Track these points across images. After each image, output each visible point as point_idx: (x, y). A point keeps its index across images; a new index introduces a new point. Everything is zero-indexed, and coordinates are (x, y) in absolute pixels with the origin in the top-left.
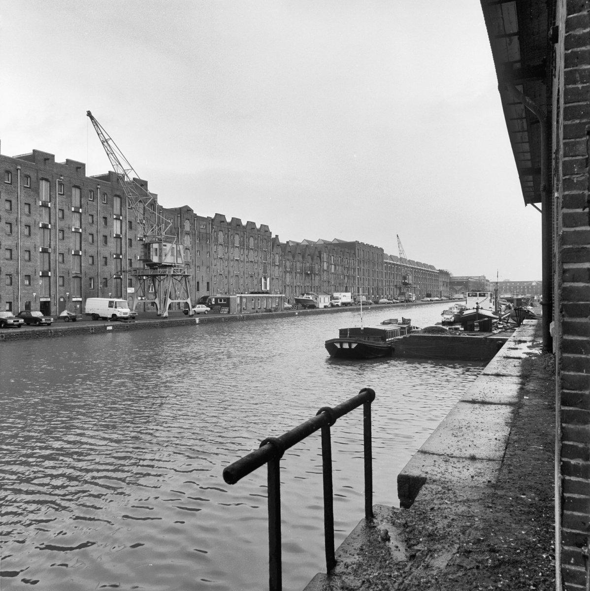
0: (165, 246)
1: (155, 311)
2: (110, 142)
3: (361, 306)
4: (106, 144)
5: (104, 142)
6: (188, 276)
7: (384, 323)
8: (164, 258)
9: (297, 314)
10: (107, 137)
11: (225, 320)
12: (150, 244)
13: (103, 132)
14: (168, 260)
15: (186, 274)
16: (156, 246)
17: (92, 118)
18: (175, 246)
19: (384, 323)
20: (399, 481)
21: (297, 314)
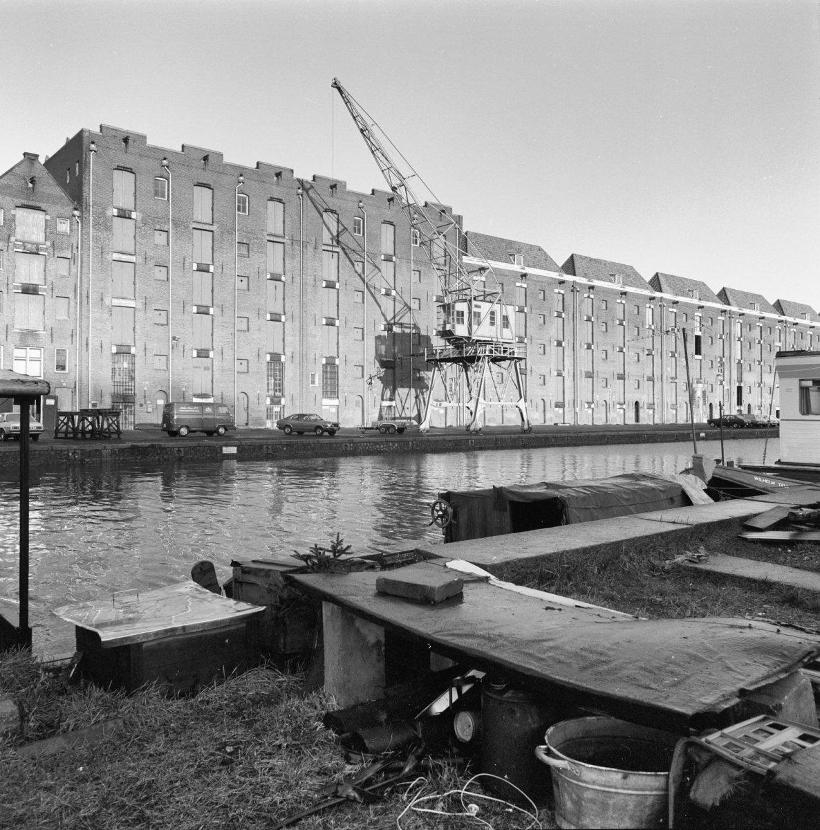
14: (483, 331)
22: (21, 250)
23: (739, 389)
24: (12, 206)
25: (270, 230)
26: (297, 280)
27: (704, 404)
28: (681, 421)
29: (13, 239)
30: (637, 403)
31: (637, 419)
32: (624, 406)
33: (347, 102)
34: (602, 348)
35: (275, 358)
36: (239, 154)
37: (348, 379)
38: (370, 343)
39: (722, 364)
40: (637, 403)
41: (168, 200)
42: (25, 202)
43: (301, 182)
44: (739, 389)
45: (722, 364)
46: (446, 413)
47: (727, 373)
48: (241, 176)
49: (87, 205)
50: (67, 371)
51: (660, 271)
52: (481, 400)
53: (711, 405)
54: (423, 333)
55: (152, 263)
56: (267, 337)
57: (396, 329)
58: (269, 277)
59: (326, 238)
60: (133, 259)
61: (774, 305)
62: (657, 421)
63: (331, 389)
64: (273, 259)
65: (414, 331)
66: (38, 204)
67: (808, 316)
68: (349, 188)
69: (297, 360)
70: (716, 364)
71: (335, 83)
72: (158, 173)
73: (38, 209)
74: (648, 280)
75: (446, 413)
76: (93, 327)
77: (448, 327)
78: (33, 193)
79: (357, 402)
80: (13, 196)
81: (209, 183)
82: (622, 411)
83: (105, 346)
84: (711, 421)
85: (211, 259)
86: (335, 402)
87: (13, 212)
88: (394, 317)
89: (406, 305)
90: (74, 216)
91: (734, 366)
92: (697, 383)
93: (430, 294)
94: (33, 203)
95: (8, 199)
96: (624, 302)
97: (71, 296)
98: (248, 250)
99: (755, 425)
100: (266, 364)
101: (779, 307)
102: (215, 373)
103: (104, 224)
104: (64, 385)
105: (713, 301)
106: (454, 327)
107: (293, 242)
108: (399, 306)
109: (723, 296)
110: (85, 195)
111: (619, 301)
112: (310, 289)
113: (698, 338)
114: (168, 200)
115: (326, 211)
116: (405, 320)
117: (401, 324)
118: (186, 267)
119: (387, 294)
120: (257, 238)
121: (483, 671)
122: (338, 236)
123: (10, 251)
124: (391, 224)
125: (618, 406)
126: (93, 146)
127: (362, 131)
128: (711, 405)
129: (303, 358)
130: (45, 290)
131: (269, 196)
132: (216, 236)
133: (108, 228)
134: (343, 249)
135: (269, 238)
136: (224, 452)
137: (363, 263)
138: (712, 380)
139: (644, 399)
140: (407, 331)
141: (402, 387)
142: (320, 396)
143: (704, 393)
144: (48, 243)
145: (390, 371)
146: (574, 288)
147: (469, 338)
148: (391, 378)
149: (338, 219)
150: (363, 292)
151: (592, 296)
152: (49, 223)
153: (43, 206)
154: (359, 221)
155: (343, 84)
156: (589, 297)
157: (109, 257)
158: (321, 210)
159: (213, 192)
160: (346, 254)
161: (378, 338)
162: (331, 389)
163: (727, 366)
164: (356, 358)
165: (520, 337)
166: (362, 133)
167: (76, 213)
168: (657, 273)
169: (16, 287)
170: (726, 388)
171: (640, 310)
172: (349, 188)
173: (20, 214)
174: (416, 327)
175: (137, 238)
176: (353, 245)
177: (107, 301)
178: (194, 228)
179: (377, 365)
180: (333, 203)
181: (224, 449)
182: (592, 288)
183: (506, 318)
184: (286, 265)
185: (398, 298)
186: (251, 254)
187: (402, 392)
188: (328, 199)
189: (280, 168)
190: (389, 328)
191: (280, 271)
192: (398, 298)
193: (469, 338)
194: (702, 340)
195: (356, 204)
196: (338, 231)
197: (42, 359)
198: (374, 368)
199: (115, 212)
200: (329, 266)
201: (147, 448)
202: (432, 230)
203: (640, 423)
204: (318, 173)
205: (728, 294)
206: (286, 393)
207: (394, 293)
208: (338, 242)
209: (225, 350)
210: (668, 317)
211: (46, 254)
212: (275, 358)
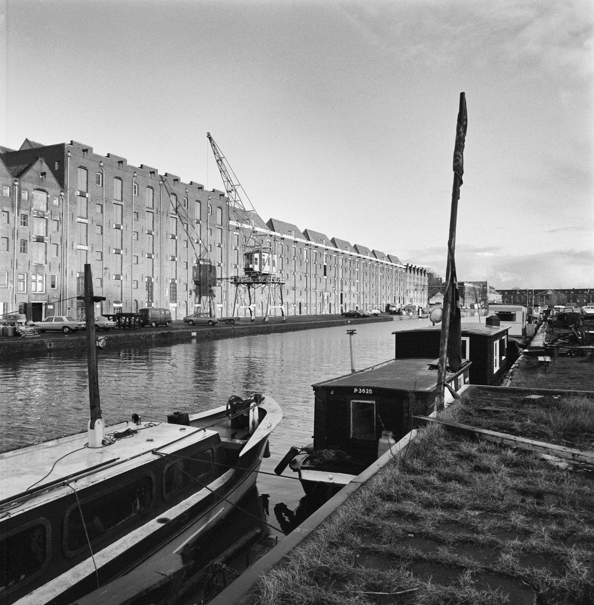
0: (264, 256)
1: (250, 316)
2: (224, 160)
3: (23, 221)
4: (220, 162)
5: (219, 160)
6: (283, 284)
7: (184, 429)
8: (263, 266)
9: (349, 322)
10: (222, 156)
11: (157, 325)
12: (252, 253)
13: (220, 152)
14: (266, 269)
15: (281, 282)
16: (257, 256)
17: (210, 138)
18: (271, 256)
19: (184, 429)
20: (486, 320)
21: (349, 322)
22: (36, 216)
23: (342, 294)
24: (32, 189)
25: (147, 205)
26: (159, 234)
27: (328, 303)
28: (313, 313)
29: (32, 209)
30: (300, 303)
31: (300, 313)
32: (295, 305)
33: (213, 145)
34: (286, 272)
35: (150, 279)
36: (134, 161)
37: (181, 294)
38: (190, 270)
39: (335, 281)
40: (300, 303)
41: (102, 186)
42: (38, 187)
43: (161, 177)
44: (342, 294)
45: (335, 281)
46: (222, 311)
47: (337, 286)
48: (135, 173)
49: (67, 188)
50: (56, 289)
51: (273, 218)
52: (269, 305)
53: (330, 304)
54: (213, 265)
55: (95, 224)
56: (144, 269)
57: (201, 263)
58: (147, 232)
59: (172, 210)
60: (86, 221)
61: (303, 233)
62: (309, 314)
63: (174, 298)
64: (147, 221)
65: (209, 264)
66: (44, 188)
67: (293, 232)
68: (95, 152)
69: (159, 280)
70: (333, 281)
71: (209, 135)
72: (98, 170)
73: (44, 191)
74: (302, 232)
75: (222, 311)
76: (69, 262)
77: (251, 266)
78: (42, 181)
79: (184, 305)
80: (33, 183)
81: (121, 176)
82: (294, 308)
83: (74, 273)
84: (343, 314)
85: (121, 222)
86: (175, 305)
87: (33, 193)
88: (200, 256)
89: (206, 249)
90: (61, 195)
91: (340, 282)
92: (325, 292)
93: (111, 222)
94: (41, 188)
95: (31, 184)
96: (295, 247)
97: (59, 243)
98: (138, 217)
99: (364, 316)
100: (145, 283)
101: (306, 234)
102: (123, 289)
103: (74, 202)
104: (55, 296)
105: (261, 227)
106: (254, 266)
107: (156, 212)
108: (203, 249)
109: (271, 225)
110: (65, 183)
111: (293, 246)
112: (164, 238)
113: (325, 266)
114: (102, 186)
115: (172, 194)
116: (205, 257)
117: (203, 260)
118: (111, 226)
119: (198, 243)
120: (141, 210)
121: (497, 373)
122: (176, 208)
123: (31, 217)
124: (85, 169)
125: (293, 305)
126: (69, 154)
127: (217, 161)
128: (330, 304)
129: (161, 280)
130: (47, 240)
131: (115, 176)
132: (124, 208)
133: (75, 203)
134: (179, 216)
135: (147, 210)
136: (192, 335)
137: (187, 224)
138: (330, 290)
139: (303, 301)
140: (206, 263)
141: (204, 295)
142: (169, 301)
143: (328, 297)
144: (49, 212)
145: (198, 287)
146: (275, 239)
147: (260, 272)
148: (198, 291)
149: (176, 198)
150: (187, 242)
151: (282, 243)
152: (49, 200)
153: (47, 189)
154: (185, 200)
155: (212, 136)
156: (281, 244)
157: (76, 220)
158: (170, 193)
159: (122, 182)
160: (180, 219)
161: (194, 267)
162: (174, 298)
163: (337, 282)
164: (184, 280)
165: (280, 270)
166: (217, 161)
167: (62, 194)
168: (271, 220)
169: (34, 238)
170: (336, 294)
171: (289, 248)
172: (95, 152)
173: (35, 193)
174: (210, 262)
175: (88, 209)
176: (183, 214)
177: (75, 247)
178: (147, 211)
179: (193, 283)
180: (175, 189)
181: (192, 333)
182: (283, 239)
183: (274, 262)
184: (154, 225)
185: (202, 244)
186: (139, 219)
187: (204, 298)
188: (173, 187)
189: (154, 169)
190: (198, 263)
191: (151, 229)
192: (202, 244)
193: (260, 272)
194: (327, 267)
195: (184, 190)
196: (176, 205)
197: (44, 281)
198: (192, 286)
199: (79, 193)
200: (171, 225)
201: (166, 334)
202: (221, 206)
203: (302, 315)
204: (169, 172)
205: (308, 233)
206: (154, 300)
207: (200, 242)
208: (177, 212)
209: (128, 275)
210: (232, 238)
211: (48, 218)
212: (150, 279)
